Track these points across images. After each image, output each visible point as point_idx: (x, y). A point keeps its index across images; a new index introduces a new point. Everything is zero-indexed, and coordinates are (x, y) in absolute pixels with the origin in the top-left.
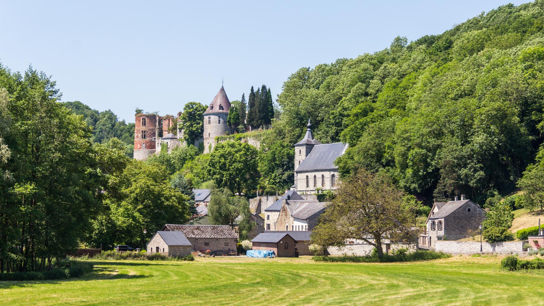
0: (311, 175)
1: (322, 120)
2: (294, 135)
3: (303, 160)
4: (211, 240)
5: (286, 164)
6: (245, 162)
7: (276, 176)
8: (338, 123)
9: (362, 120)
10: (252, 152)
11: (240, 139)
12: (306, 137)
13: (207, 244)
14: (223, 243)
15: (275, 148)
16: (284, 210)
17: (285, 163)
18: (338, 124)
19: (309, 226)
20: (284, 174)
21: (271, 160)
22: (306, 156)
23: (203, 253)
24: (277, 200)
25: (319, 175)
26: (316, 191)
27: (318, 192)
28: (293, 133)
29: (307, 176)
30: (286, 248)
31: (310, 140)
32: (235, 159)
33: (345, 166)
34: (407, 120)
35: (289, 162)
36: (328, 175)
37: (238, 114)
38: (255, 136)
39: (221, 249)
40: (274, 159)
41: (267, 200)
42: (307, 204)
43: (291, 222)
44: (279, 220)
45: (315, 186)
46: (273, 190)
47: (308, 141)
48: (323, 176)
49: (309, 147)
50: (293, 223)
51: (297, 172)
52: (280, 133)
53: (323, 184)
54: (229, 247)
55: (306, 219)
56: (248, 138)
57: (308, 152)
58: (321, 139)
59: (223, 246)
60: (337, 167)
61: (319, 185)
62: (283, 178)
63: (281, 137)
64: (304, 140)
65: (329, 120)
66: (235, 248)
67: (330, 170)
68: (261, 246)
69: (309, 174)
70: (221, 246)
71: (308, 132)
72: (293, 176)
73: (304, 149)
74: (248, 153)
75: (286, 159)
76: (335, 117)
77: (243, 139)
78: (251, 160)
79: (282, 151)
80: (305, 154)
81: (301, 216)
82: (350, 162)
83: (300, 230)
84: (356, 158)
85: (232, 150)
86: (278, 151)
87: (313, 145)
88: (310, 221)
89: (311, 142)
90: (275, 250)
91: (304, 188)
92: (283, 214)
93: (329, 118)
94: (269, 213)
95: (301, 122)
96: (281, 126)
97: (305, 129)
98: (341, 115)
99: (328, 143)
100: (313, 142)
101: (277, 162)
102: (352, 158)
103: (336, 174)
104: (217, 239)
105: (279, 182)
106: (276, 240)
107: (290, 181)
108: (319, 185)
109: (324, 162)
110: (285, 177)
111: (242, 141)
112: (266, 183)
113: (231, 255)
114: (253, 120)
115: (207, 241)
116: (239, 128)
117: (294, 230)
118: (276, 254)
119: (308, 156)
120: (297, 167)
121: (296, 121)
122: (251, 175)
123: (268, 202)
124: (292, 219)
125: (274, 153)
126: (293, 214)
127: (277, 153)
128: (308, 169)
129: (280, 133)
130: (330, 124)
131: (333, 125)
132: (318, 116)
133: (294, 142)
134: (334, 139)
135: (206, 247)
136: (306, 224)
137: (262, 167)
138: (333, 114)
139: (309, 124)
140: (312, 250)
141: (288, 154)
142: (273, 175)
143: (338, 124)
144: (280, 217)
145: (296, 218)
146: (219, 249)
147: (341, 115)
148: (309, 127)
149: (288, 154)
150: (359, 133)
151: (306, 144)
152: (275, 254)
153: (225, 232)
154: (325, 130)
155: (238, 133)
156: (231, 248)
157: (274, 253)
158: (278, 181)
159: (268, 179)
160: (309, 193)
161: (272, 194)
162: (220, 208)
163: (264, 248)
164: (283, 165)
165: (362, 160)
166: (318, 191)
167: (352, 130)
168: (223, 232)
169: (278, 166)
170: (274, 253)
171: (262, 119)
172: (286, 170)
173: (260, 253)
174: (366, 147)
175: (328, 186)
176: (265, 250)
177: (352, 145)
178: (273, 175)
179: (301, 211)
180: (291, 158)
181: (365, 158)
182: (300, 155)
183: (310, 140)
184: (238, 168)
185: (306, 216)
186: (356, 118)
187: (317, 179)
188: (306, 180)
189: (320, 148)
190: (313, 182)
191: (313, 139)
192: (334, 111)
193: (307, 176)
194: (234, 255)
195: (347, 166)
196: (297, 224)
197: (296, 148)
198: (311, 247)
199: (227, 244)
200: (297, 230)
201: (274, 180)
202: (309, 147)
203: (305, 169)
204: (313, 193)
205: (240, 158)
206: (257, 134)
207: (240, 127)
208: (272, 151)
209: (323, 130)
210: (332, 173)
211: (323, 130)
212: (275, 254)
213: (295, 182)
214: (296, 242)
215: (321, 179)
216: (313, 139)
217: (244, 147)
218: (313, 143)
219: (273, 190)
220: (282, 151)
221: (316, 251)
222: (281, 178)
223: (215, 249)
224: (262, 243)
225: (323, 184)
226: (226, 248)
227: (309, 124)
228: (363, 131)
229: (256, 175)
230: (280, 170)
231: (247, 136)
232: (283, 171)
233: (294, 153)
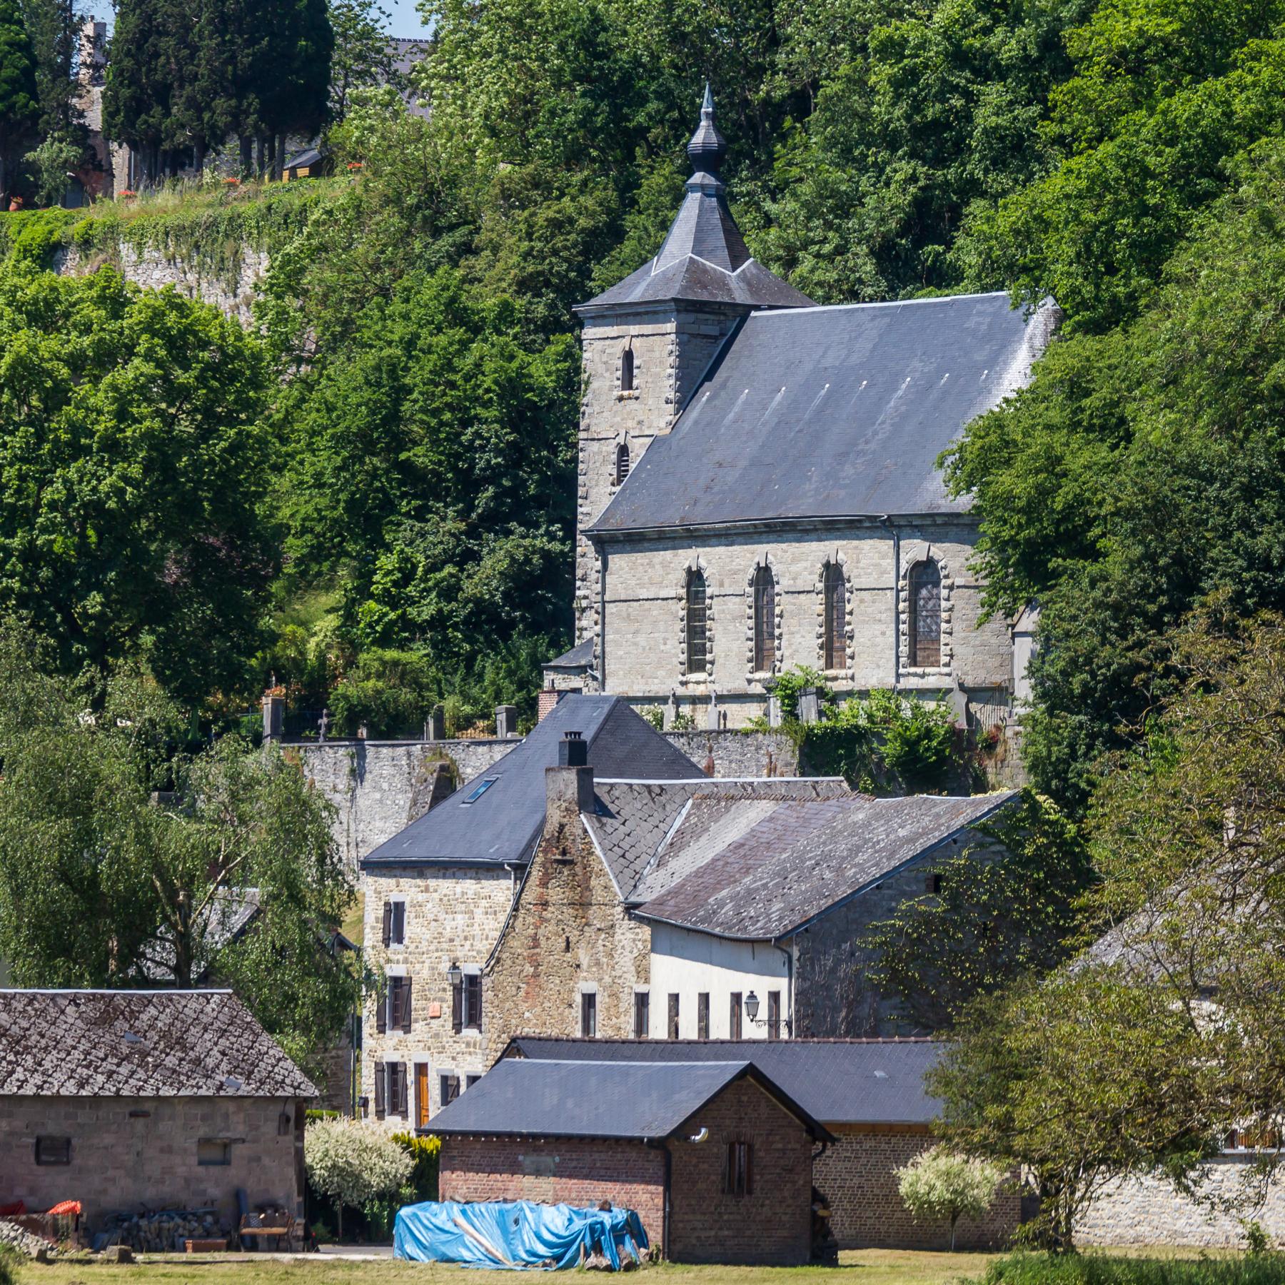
0: (729, 566)
1: (800, 103)
2: (557, 225)
3: (657, 443)
4: (84, 1116)
5: (493, 476)
6: (162, 451)
7: (407, 575)
8: (937, 126)
9: (1188, 103)
10: (212, 368)
11: (49, 255)
12: (681, 249)
13: (53, 1151)
14: (183, 1136)
15: (399, 330)
16: (566, 859)
17: (481, 461)
18: (937, 139)
19: (802, 998)
20: (476, 557)
21: (363, 435)
22: (683, 402)
23: (33, 1227)
24: (446, 784)
25: (796, 563)
26: (775, 705)
27: (791, 713)
28: (544, 214)
29: (695, 578)
30: (738, 1183)
31: (716, 266)
32: (77, 429)
33: (1044, 493)
34: (1189, 100)
35: (515, 456)
36: (873, 563)
37: (25, 48)
38: (180, 232)
39: (170, 1189)
40: (387, 430)
41: (358, 774)
42: (763, 808)
43: (626, 962)
44: (517, 944)
45: (761, 655)
46: (406, 695)
47: (695, 273)
48: (833, 575)
49: (709, 332)
50: (643, 973)
51: (606, 543)
52: (434, 209)
53: (834, 641)
54: (235, 1174)
55: (781, 942)
56: (126, 250)
57: (694, 375)
58: (791, 263)
59: (186, 1165)
60: (965, 502)
61: (799, 650)
62: (469, 588)
63: (445, 242)
64: (658, 267)
65: (857, 102)
66: (286, 1190)
67: (892, 527)
68: (515, 1168)
69: (710, 559)
70: (176, 1170)
71: (692, 202)
72: (559, 573)
73: (658, 348)
74: (183, 377)
75: (491, 428)
76: (912, 76)
77: (73, 257)
78: (205, 434)
79: (467, 362)
80: (668, 386)
81: (723, 907)
82: (1083, 456)
83: (689, 1030)
84: (1153, 424)
85: (50, 344)
86: (431, 361)
87: (742, 313)
88: (810, 958)
89: (722, 283)
90: (647, 1201)
91: (667, 680)
92: (555, 894)
93: (858, 83)
94: (406, 890)
95: (617, 116)
96: (442, 147)
97: (655, 180)
98: (959, 57)
99: (853, 295)
100: (735, 283)
101: (421, 456)
102: (1115, 428)
103: (956, 560)
104: (138, 1108)
105: (439, 622)
106: (656, 1119)
107: (542, 610)
108: (799, 650)
109: (842, 457)
110: (487, 575)
111: (75, 272)
112: (314, 624)
113: (252, 1245)
114: (163, 95)
115: (54, 1127)
116: (34, 168)
117: (658, 1029)
118: (655, 1237)
119: (695, 411)
120: (597, 500)
121: (575, 101)
122: (201, 559)
123: (372, 799)
124: (632, 937)
125: (391, 381)
126: (646, 895)
127: (416, 376)
128: (701, 516)
129: (434, 209)
130: (867, 140)
131: (893, 146)
132: (757, 73)
133: (564, 295)
134: (912, 256)
135: (52, 1178)
136: (781, 984)
137: (294, 500)
138: (892, 49)
139: (703, 136)
140: (926, 1206)
141: (513, 387)
142: (387, 561)
143: (937, 139)
144: (526, 921)
145: (675, 931)
146: (150, 1193)
147: (959, 57)
148: (708, 160)
149: (513, 387)
150: (1157, 212)
151: (684, 307)
152: (642, 1240)
153: (203, 1043)
154: (826, 190)
155: (28, 205)
156: (254, 1188)
157: (633, 1228)
158: (426, 611)
159: (335, 597)
160: (705, 718)
161: (394, 724)
162: (86, 836)
163: (548, 1184)
164: (469, 485)
165: (1203, 441)
166: (791, 698)
167: (1098, 186)
168: (181, 1043)
169: (424, 487)
170: (633, 1228)
171: (239, 87)
172: (495, 521)
173: (508, 1227)
174: (1239, 337)
175: (874, 661)
176: (551, 1210)
177: (1103, 316)
178: (387, 561)
179: (716, 873)
180: (545, 422)
181: (1227, 425)
182: (626, 397)
183: (716, 266)
184: (95, 509)
185: (773, 917)
186: (1125, 84)
187: (783, 604)
188: (680, 609)
189: (803, 342)
190: (746, 628)
191: (736, 261)
192: (908, 29)
193: (695, 578)
194: (277, 1244)
195: (1068, 491)
196: (677, 976)
197: (589, 333)
198: (924, 1176)
199: (217, 1152)
200: (689, 1030)
201: (393, 602)
202: (709, 332)
203: (672, 517)
204: (742, 716)
205: (122, 415)
206: (205, 214)
207: (43, 154)
208: (371, 358)
209: (806, 189)
210: (915, 549)
211: (806, 189)
212: (642, 1240)
213: (586, 623)
214: (820, 1133)
215: (816, 604)
216: (737, 255)
217: (152, 326)
218: (741, 297)
219: (406, 695)
220: (467, 362)
221: (954, 1210)
222: (449, 592)
223: (120, 1191)
224: (531, 1141)
225: (834, 641)
226: (215, 1185)
227: (703, 136)
228: (1198, 200)
229: (238, 562)
230: (447, 524)
231: (112, 231)
232: (472, 532)
233: (572, 381)
